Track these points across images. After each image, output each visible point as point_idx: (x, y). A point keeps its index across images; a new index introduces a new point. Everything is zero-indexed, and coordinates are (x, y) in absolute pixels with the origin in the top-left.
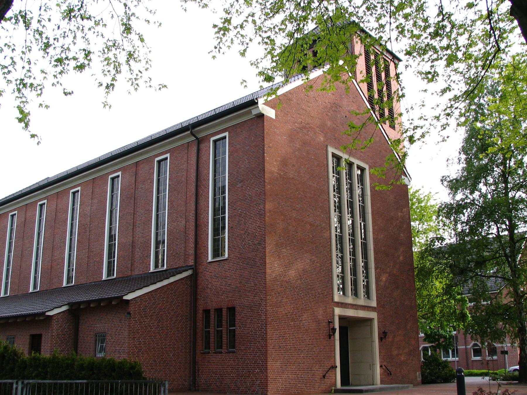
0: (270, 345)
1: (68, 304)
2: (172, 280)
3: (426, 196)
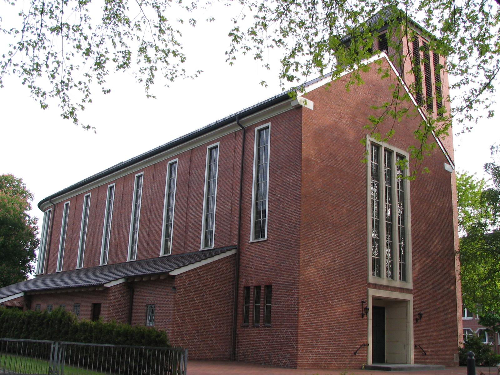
0: (301, 321)
1: (124, 277)
2: (216, 258)
3: (479, 182)
